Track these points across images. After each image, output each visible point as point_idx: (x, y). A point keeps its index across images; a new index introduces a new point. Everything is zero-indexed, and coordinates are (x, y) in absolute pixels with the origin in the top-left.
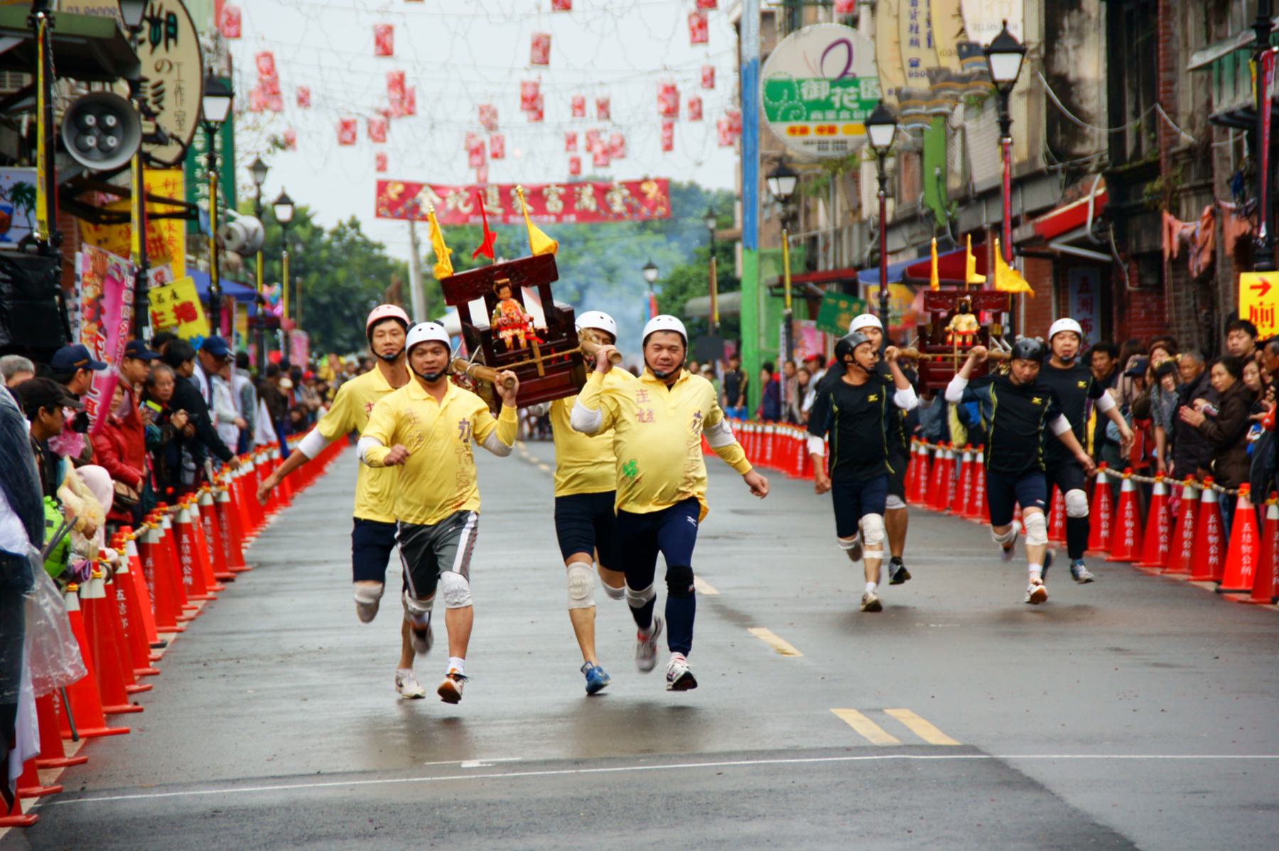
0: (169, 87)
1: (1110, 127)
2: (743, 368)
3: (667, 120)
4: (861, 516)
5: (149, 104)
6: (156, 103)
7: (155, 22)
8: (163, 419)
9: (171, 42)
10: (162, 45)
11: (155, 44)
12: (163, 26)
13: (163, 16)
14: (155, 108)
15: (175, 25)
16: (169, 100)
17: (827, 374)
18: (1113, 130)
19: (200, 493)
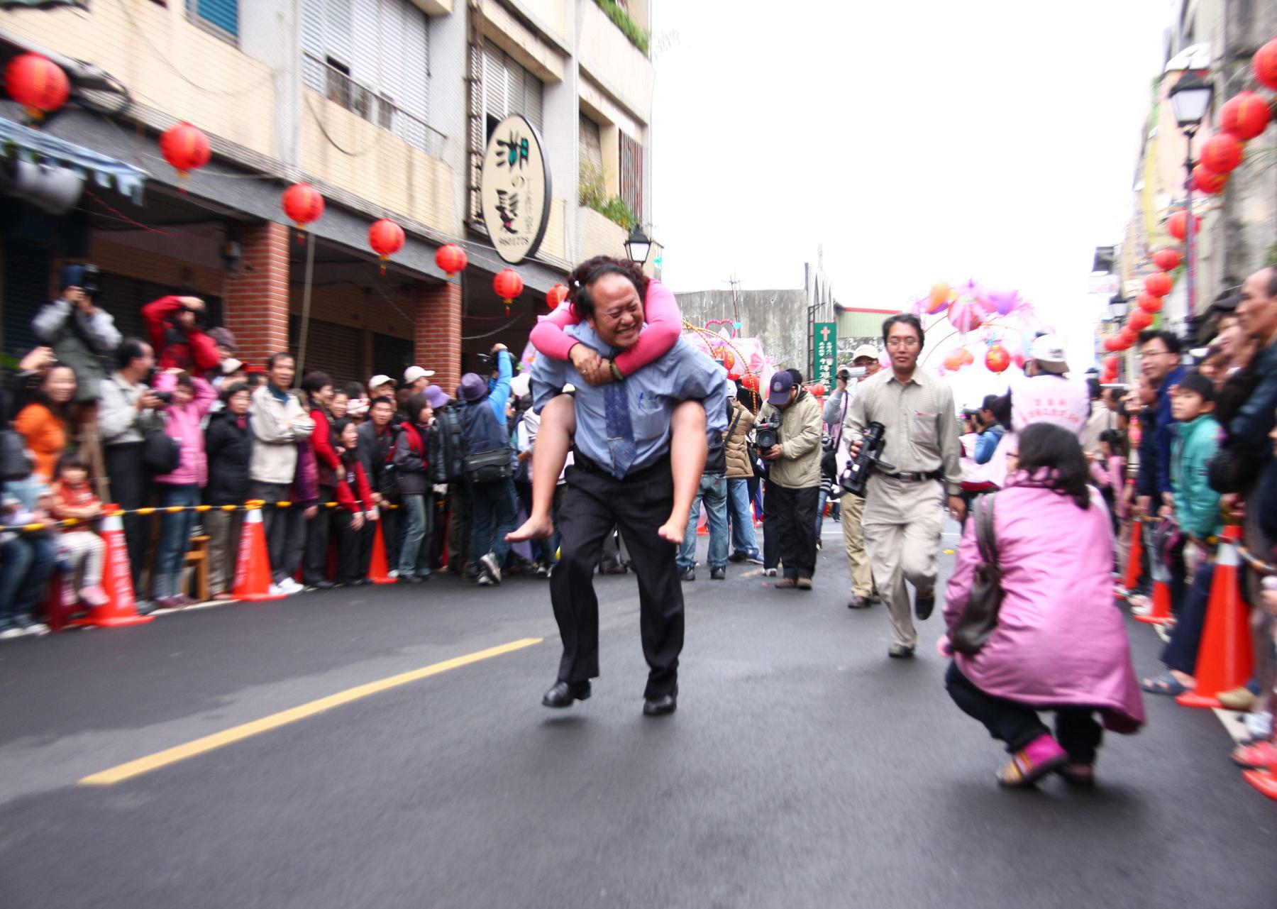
0: (521, 199)
1: (317, 237)
2: (920, 361)
3: (1161, 276)
4: (405, 368)
5: (507, 212)
6: (512, 211)
7: (512, 146)
8: (121, 360)
9: (524, 161)
10: (517, 165)
11: (512, 164)
12: (518, 150)
13: (519, 142)
14: (510, 215)
15: (527, 149)
16: (520, 210)
17: (108, 310)
18: (312, 240)
19: (394, 401)
